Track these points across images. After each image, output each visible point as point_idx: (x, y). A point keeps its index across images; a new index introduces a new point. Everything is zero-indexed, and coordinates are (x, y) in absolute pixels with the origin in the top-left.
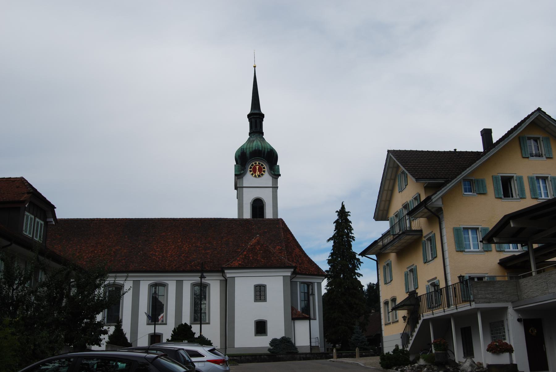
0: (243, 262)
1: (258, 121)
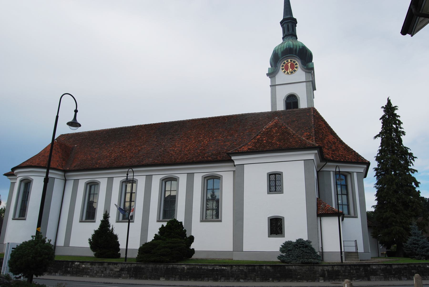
0: (253, 146)
1: (290, 25)
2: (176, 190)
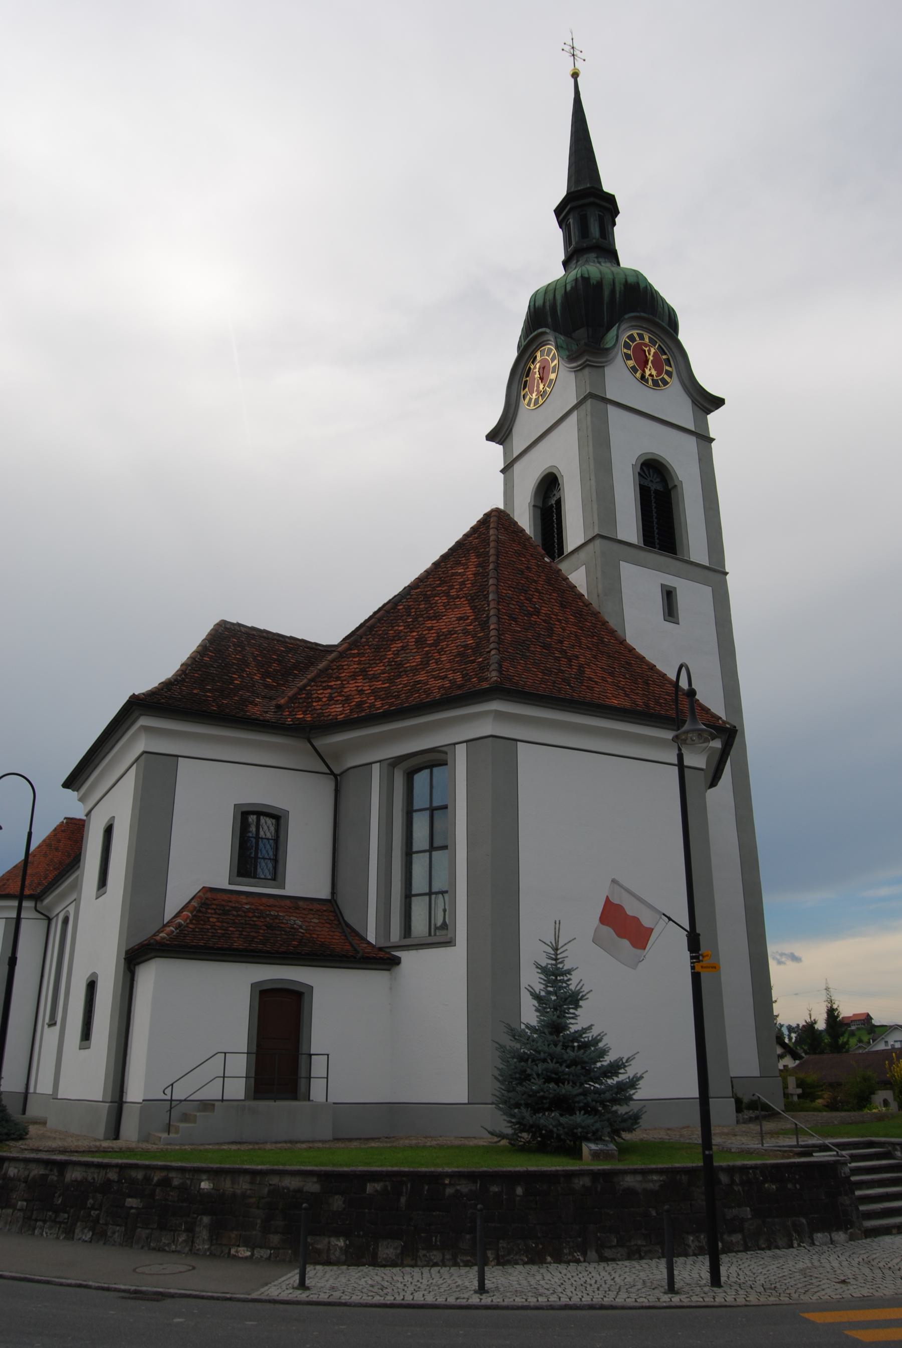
2: (327, 1100)
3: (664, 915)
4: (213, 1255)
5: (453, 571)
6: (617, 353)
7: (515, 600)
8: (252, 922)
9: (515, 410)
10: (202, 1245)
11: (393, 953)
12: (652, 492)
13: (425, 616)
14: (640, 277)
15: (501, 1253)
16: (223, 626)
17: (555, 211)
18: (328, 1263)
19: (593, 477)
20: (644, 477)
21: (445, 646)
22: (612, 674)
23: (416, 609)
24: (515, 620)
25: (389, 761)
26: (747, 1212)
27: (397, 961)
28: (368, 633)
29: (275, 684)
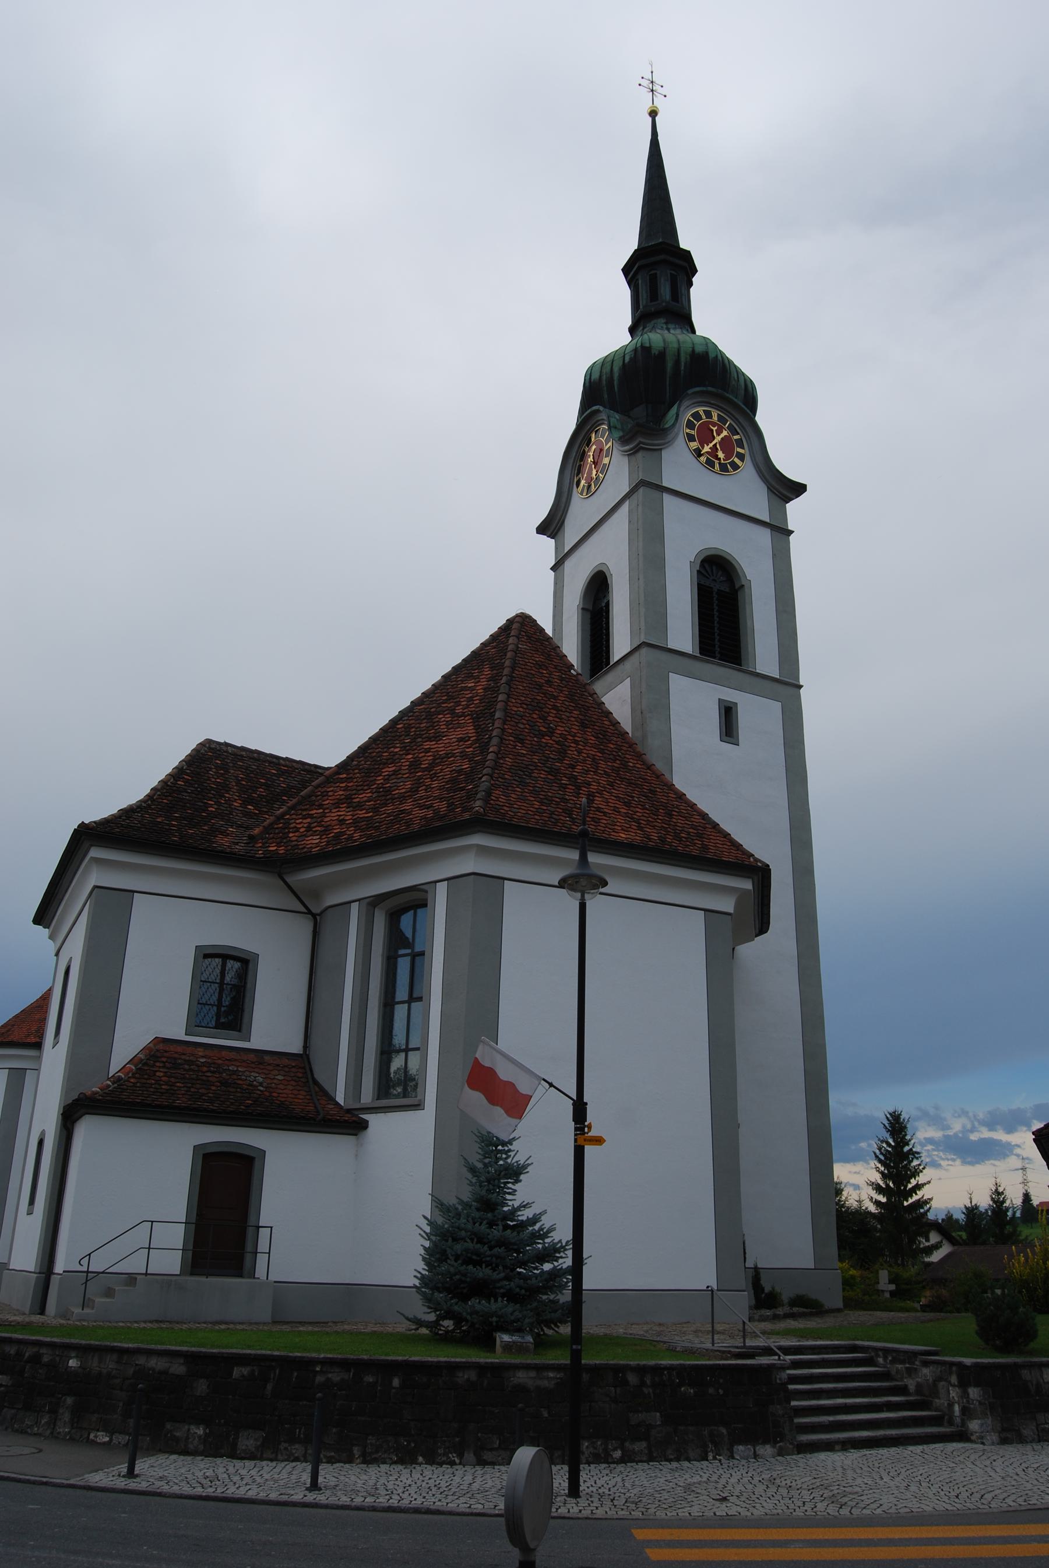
2: (267, 1279)
3: (544, 1080)
4: (72, 1439)
5: (463, 685)
6: (677, 434)
7: (527, 719)
8: (204, 1078)
9: (567, 498)
10: (64, 1429)
11: (361, 1116)
12: (714, 593)
13: (424, 736)
14: (710, 345)
15: (369, 1450)
16: (207, 745)
17: (623, 270)
18: (185, 1452)
19: (641, 577)
20: (705, 576)
21: (438, 771)
22: (628, 804)
23: (417, 728)
24: (522, 741)
25: (368, 900)
26: (656, 1417)
27: (363, 1126)
28: (361, 755)
29: (257, 812)
